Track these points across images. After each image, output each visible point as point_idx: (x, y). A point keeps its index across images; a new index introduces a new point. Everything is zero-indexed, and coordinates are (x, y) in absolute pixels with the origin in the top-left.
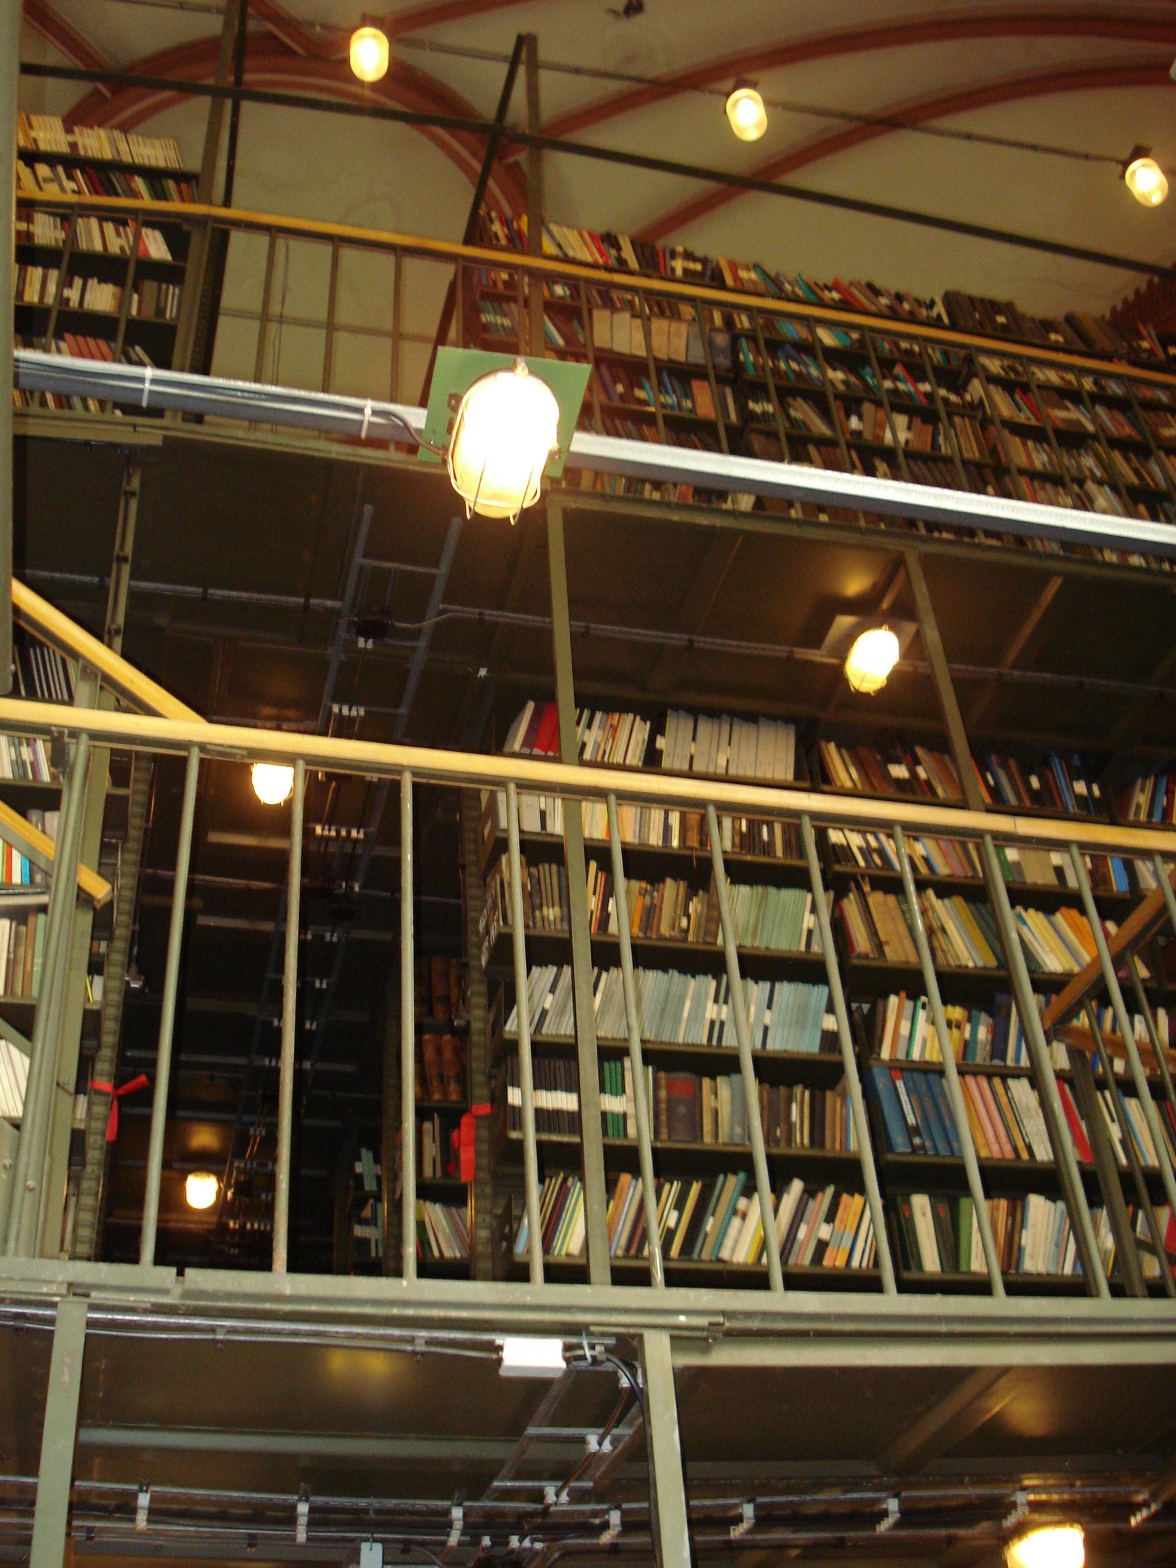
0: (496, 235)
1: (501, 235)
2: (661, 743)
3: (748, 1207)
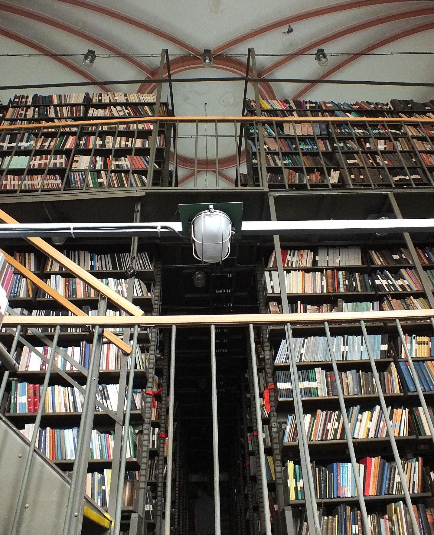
1: (254, 105)
2: (317, 258)
3: (362, 417)
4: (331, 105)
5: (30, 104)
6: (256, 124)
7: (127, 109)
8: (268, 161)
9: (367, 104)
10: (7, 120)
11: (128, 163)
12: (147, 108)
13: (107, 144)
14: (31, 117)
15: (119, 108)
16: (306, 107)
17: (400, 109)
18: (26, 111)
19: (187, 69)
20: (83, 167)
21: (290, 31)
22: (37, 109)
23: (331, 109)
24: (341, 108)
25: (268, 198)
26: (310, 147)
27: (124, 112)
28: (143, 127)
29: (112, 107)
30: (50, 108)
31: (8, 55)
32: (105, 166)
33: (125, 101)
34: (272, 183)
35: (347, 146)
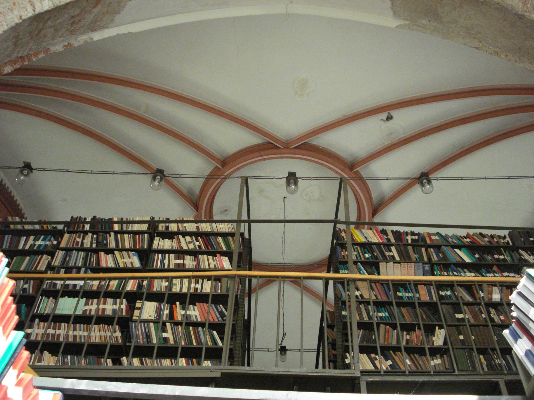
0: (343, 237)
1: (345, 237)
4: (437, 238)
5: (88, 229)
6: (348, 285)
7: (197, 240)
8: (360, 314)
9: (481, 237)
10: (62, 249)
11: (197, 313)
12: (220, 239)
13: (174, 287)
14: (89, 246)
15: (188, 238)
16: (407, 240)
17: (519, 244)
18: (84, 238)
19: (264, 159)
20: (145, 316)
21: (389, 118)
22: (95, 236)
23: (436, 243)
24: (448, 241)
25: (359, 383)
26: (410, 295)
27: (194, 244)
28: (215, 265)
29: (180, 237)
30: (110, 236)
31: (67, 171)
32: (172, 315)
33: (195, 230)
34: (365, 344)
35: (455, 295)
